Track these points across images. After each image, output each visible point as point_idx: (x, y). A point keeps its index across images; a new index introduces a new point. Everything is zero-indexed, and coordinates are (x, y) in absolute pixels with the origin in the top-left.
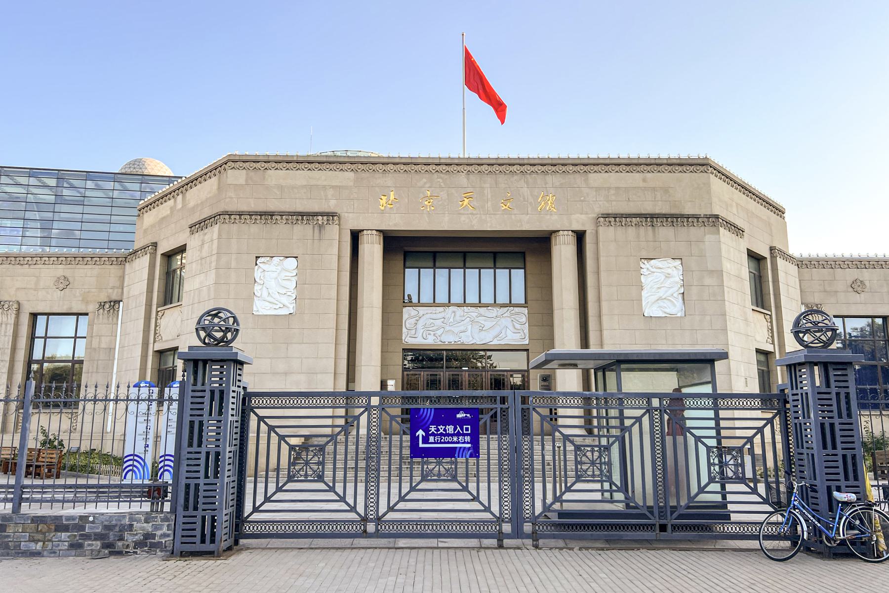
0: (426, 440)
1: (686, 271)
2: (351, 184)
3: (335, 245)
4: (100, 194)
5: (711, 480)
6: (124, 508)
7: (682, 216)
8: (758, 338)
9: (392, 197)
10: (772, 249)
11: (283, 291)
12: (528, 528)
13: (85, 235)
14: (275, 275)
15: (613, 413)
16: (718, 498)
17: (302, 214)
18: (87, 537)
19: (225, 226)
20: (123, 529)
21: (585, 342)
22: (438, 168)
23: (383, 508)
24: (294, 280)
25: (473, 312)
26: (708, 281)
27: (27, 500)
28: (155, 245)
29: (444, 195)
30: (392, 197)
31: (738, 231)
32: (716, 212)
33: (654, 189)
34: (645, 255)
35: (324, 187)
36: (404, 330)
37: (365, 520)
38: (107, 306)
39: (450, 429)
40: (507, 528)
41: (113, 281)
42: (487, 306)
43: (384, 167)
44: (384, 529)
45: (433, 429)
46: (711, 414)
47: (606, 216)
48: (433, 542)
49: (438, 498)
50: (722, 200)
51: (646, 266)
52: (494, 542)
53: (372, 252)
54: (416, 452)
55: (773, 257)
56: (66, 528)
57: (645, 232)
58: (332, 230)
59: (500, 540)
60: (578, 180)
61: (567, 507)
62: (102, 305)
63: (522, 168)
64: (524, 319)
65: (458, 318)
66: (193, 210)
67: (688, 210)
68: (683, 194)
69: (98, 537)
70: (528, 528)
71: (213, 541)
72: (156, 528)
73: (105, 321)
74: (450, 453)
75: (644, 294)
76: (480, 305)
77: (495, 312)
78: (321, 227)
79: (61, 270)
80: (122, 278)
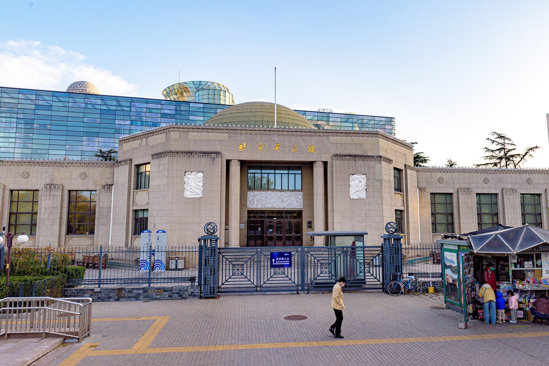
0: (275, 262)
1: (368, 180)
2: (227, 139)
3: (219, 167)
4: (60, 104)
5: (361, 272)
6: (183, 284)
7: (367, 156)
8: (397, 205)
9: (245, 145)
10: (405, 165)
11: (197, 187)
12: (306, 288)
13: (53, 128)
14: (193, 180)
15: (333, 253)
16: (363, 278)
17: (205, 153)
18: (174, 293)
19: (171, 158)
20: (185, 291)
21: (327, 229)
22: (265, 132)
23: (262, 283)
24: (202, 182)
25: (279, 194)
26: (377, 184)
27: (152, 283)
28: (131, 160)
29: (267, 144)
30: (245, 145)
31: (390, 161)
32: (381, 155)
33: (356, 144)
34: (351, 173)
35: (214, 140)
36: (248, 202)
37: (257, 287)
38: (106, 187)
39: (283, 259)
40: (300, 288)
41: (108, 175)
42: (285, 191)
43: (241, 132)
44: (262, 289)
45: (277, 259)
46: (362, 252)
47: (336, 155)
48: (277, 293)
49: (279, 278)
50: (384, 148)
51: (352, 177)
52: (296, 292)
53: (235, 169)
54: (272, 266)
55: (406, 169)
56: (167, 291)
57: (352, 162)
58: (218, 160)
59: (298, 292)
60: (325, 139)
61: (318, 281)
62: (104, 187)
63: (301, 133)
64: (301, 197)
65: (272, 196)
66: (153, 146)
67: (370, 154)
68: (367, 146)
69: (177, 293)
70: (306, 288)
71: (214, 294)
72: (195, 290)
73: (106, 194)
74: (283, 266)
75: (351, 189)
76: (282, 190)
77: (288, 193)
78: (213, 159)
79: (82, 170)
80: (113, 173)
